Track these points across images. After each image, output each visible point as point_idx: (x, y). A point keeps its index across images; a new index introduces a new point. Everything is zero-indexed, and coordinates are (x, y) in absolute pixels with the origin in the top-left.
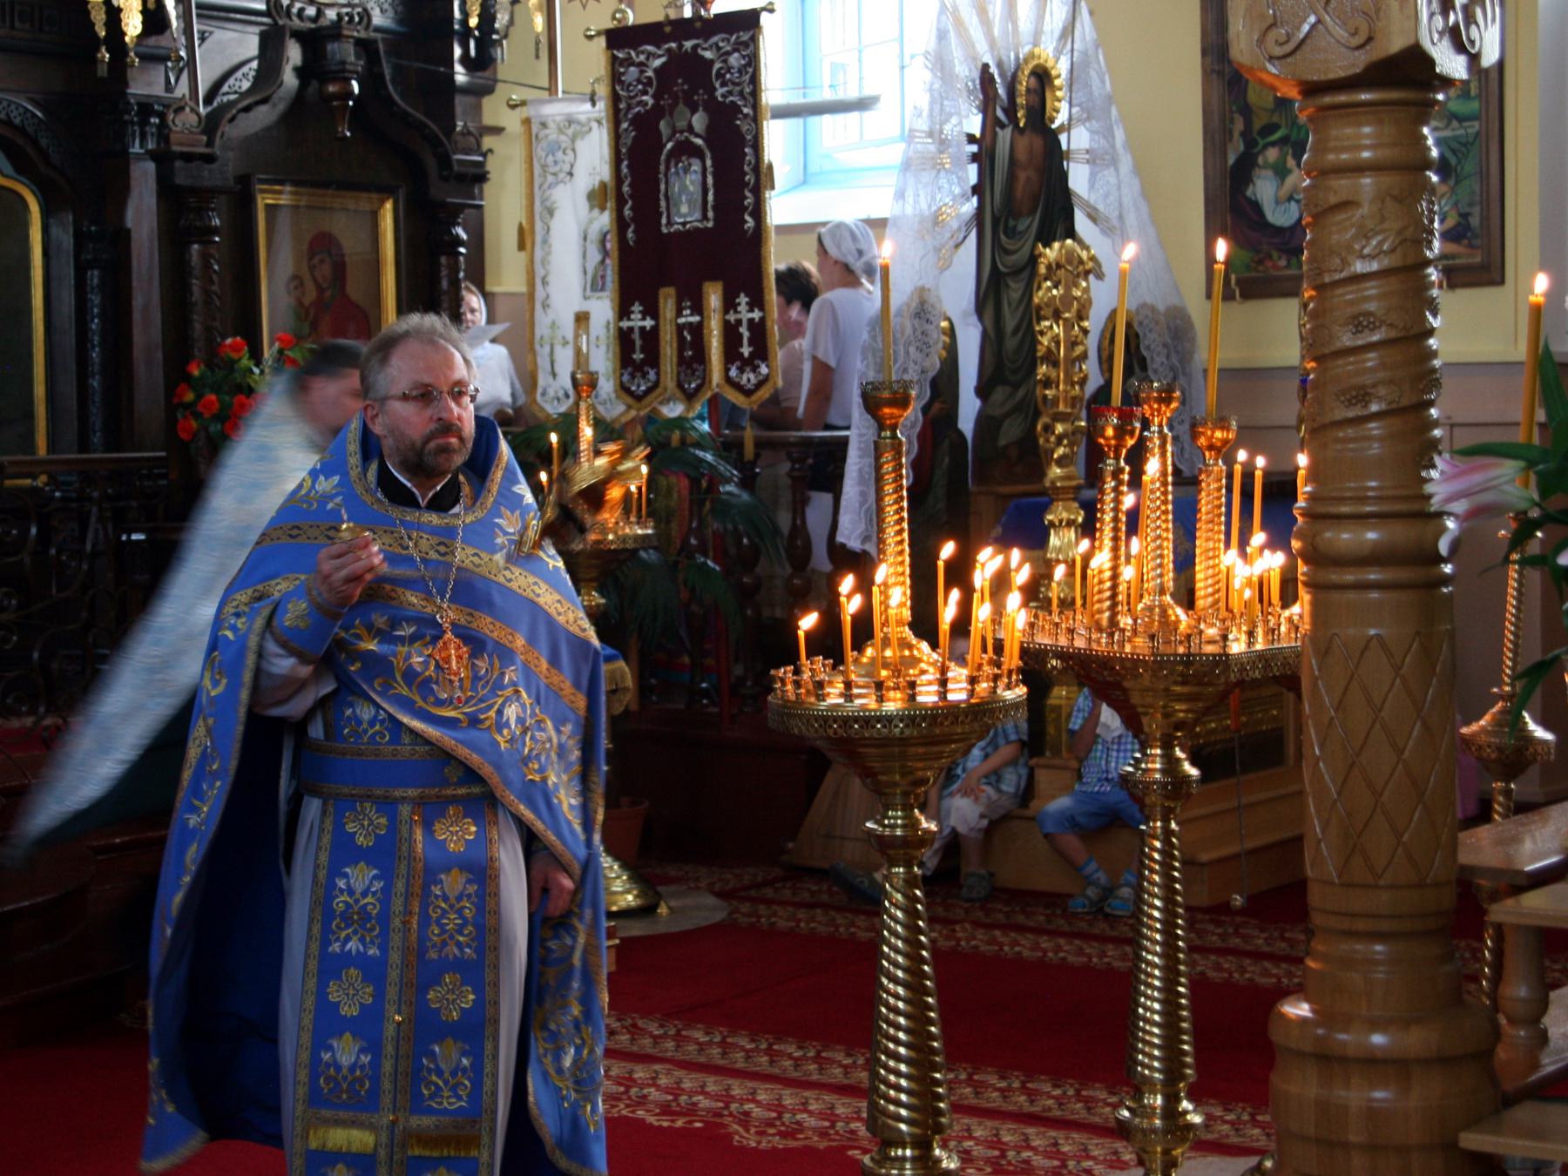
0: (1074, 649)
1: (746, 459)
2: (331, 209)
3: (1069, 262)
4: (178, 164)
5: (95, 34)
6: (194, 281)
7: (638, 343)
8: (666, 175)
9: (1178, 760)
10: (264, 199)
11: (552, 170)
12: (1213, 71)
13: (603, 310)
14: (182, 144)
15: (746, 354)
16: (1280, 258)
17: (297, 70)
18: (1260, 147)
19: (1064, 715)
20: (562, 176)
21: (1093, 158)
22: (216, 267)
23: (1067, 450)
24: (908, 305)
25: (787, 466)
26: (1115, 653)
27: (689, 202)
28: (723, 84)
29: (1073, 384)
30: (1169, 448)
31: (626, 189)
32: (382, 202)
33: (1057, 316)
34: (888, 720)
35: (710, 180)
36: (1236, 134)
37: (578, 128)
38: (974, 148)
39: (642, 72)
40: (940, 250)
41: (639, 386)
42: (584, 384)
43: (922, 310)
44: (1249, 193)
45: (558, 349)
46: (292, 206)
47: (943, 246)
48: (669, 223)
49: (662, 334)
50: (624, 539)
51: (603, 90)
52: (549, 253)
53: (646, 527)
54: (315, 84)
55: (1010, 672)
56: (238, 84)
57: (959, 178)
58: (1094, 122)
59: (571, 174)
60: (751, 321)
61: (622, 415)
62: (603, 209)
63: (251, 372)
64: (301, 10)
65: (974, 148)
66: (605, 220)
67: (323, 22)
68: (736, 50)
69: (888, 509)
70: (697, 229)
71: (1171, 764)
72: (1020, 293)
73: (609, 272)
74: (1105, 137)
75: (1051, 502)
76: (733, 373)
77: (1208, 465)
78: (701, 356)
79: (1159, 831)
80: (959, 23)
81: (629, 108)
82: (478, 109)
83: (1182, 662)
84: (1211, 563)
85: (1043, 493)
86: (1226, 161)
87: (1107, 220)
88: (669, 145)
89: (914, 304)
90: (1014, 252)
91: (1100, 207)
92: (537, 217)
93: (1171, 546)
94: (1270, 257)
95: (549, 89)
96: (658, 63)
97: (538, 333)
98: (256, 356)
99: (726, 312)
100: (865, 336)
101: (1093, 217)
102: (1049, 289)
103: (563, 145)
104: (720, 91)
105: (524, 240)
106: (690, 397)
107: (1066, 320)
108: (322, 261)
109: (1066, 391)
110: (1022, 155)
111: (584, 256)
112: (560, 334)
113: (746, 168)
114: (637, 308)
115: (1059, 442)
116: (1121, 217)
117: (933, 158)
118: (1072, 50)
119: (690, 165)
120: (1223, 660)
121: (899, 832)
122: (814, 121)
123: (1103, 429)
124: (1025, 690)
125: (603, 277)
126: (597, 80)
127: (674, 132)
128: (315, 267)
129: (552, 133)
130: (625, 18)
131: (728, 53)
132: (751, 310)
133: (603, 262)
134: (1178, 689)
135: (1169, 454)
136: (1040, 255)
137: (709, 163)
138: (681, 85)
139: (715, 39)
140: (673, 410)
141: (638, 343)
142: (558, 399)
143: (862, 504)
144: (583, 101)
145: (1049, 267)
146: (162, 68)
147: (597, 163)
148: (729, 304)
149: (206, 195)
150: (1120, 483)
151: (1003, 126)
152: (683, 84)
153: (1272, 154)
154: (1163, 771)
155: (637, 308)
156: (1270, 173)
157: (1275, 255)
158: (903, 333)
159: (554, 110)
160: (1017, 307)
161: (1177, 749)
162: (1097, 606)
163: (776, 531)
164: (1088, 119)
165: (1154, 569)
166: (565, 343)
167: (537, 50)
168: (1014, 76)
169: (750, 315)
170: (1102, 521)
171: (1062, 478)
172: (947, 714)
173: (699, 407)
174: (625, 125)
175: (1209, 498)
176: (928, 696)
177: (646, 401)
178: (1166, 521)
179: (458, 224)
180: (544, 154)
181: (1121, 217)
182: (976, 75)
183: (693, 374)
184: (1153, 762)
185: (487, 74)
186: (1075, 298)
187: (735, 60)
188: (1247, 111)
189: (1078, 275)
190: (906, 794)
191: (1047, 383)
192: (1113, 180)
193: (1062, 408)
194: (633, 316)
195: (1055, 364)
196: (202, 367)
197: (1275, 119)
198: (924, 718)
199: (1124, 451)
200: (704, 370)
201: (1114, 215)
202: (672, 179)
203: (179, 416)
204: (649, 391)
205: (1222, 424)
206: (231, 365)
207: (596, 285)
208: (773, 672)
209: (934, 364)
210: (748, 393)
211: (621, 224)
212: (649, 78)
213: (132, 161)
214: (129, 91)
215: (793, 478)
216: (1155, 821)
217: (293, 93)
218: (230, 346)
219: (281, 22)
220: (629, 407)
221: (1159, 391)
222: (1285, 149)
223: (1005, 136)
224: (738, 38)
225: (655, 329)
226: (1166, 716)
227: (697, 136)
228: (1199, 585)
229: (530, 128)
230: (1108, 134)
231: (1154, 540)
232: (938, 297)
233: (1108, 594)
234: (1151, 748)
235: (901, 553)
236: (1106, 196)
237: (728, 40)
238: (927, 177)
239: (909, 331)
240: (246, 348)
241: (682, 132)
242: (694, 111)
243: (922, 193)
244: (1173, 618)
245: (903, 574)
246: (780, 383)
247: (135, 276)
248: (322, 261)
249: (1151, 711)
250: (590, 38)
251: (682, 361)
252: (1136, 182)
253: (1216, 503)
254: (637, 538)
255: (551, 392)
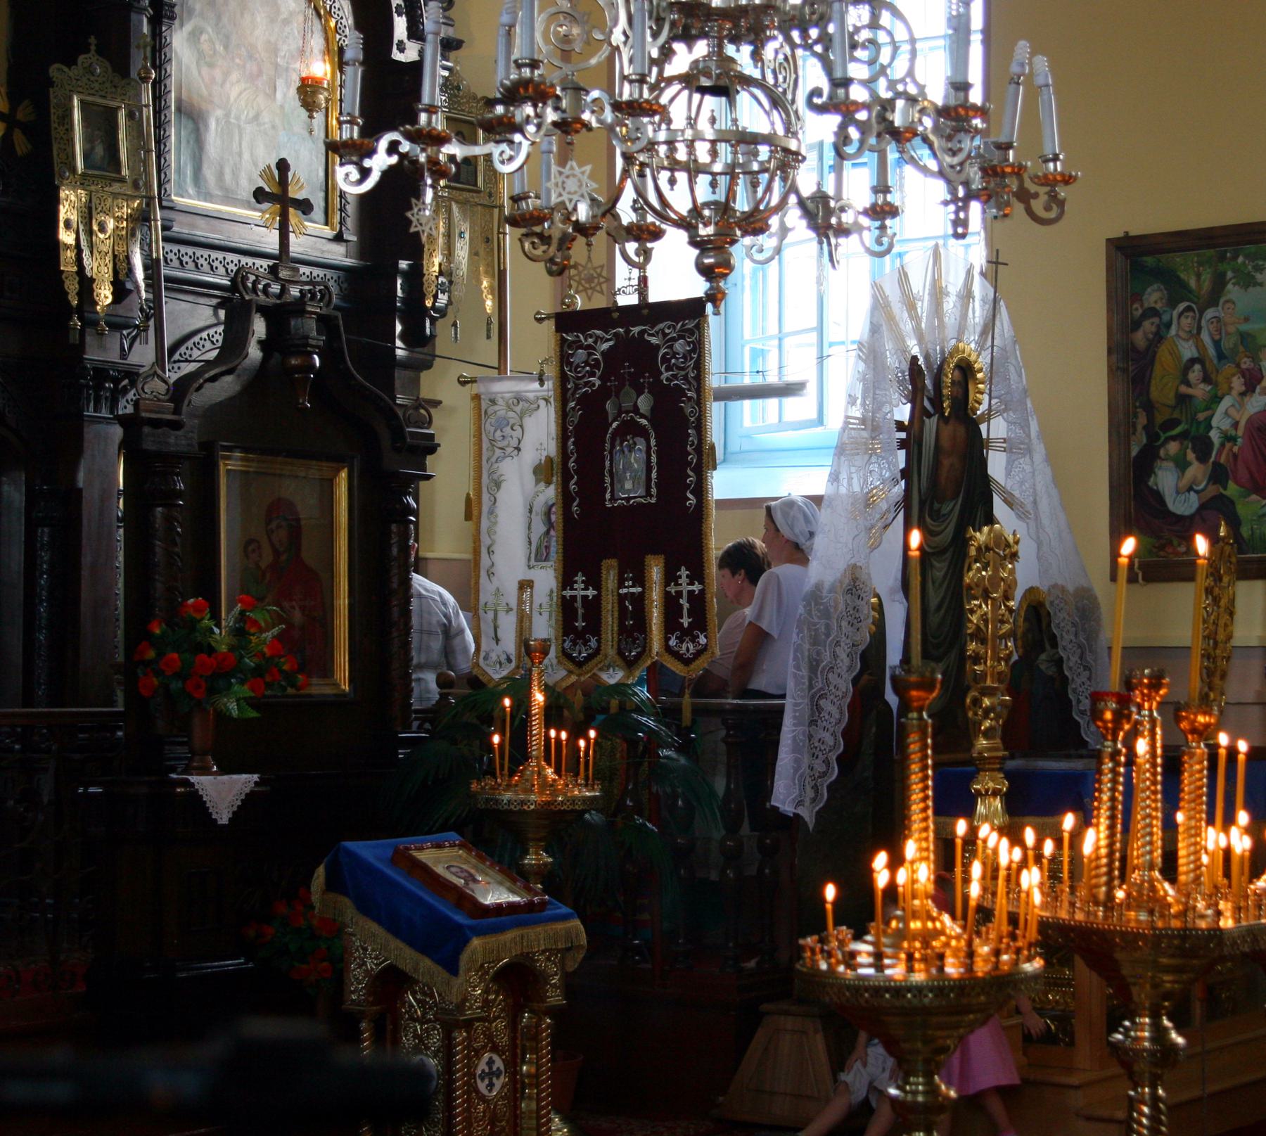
0: (1075, 921)
1: (684, 724)
2: (280, 475)
3: (998, 545)
4: (146, 430)
5: (68, 302)
6: (158, 543)
7: (686, 606)
8: (611, 453)
9: (1166, 1029)
10: (227, 465)
11: (500, 444)
12: (1118, 368)
13: (546, 579)
14: (151, 411)
15: (686, 625)
16: (1179, 545)
17: (260, 342)
18: (1162, 439)
19: (574, 936)
20: (509, 450)
21: (1009, 446)
22: (179, 530)
23: (993, 723)
24: (841, 582)
25: (723, 733)
26: (1115, 926)
27: (633, 479)
28: (667, 370)
29: (999, 660)
30: (1158, 731)
31: (571, 464)
32: (338, 471)
33: (986, 596)
34: (918, 990)
35: (654, 459)
36: (1139, 427)
37: (526, 405)
38: (903, 435)
39: (590, 354)
40: (870, 529)
41: (580, 653)
42: (529, 650)
43: (854, 585)
44: (1151, 483)
45: (501, 615)
46: (242, 472)
47: (873, 527)
48: (613, 499)
49: (604, 603)
50: (573, 800)
51: (551, 371)
52: (496, 523)
53: (593, 790)
54: (277, 357)
55: (1030, 945)
56: (188, 352)
57: (889, 463)
58: (1011, 413)
59: (518, 449)
60: (691, 593)
61: (562, 679)
62: (548, 483)
63: (212, 632)
64: (267, 286)
65: (903, 435)
66: (550, 493)
67: (287, 299)
68: (682, 337)
69: (914, 787)
70: (640, 504)
71: (1159, 1034)
72: (942, 573)
73: (553, 543)
74: (1022, 428)
75: (978, 771)
76: (673, 642)
77: (1190, 747)
78: (642, 624)
79: (1147, 1097)
80: (891, 318)
81: (577, 387)
82: (416, 382)
83: (1179, 936)
84: (1193, 840)
85: (971, 762)
86: (1129, 453)
87: (1022, 505)
88: (615, 425)
89: (847, 581)
90: (938, 534)
91: (1016, 493)
92: (484, 489)
93: (1159, 824)
94: (1171, 543)
95: (498, 369)
96: (605, 346)
97: (482, 600)
98: (216, 616)
99: (667, 584)
100: (801, 610)
101: (1009, 502)
102: (979, 570)
103: (512, 421)
104: (665, 375)
105: (471, 510)
106: (630, 664)
107: (993, 599)
108: (279, 527)
109: (993, 667)
110: (946, 443)
111: (529, 528)
112: (503, 601)
113: (689, 448)
114: (580, 578)
115: (986, 716)
116: (1035, 502)
117: (865, 444)
118: (993, 346)
119: (635, 444)
120: (1216, 934)
121: (920, 1099)
122: (734, 405)
123: (1102, 713)
124: (1042, 962)
125: (547, 548)
126: (546, 361)
127: (620, 413)
128: (273, 532)
129: (501, 409)
130: (574, 304)
131: (674, 340)
132: (692, 583)
133: (547, 532)
134: (1164, 960)
135: (1158, 737)
136: (971, 538)
137: (653, 442)
138: (627, 369)
139: (661, 326)
140: (613, 677)
141: (580, 611)
142: (500, 664)
143: (796, 770)
144: (532, 380)
145: (979, 549)
146: (118, 335)
147: (544, 439)
148: (670, 576)
149: (170, 459)
150: (1118, 764)
151: (929, 416)
152: (629, 367)
153: (1173, 447)
154: (1153, 1040)
155: (580, 578)
156: (1171, 465)
157: (1175, 542)
158: (836, 607)
159: (504, 388)
160: (941, 585)
161: (1164, 1018)
162: (1094, 881)
163: (713, 794)
164: (1005, 410)
165: (1144, 846)
166: (509, 610)
167: (489, 331)
168: (941, 368)
169: (691, 588)
170: (1099, 800)
171: (989, 750)
172: (967, 985)
173: (640, 672)
174: (572, 404)
175: (1194, 774)
176: (952, 969)
177: (586, 668)
178: (1155, 801)
179: (409, 494)
180: (492, 429)
181: (1035, 502)
182: (906, 366)
183: (634, 642)
184: (1143, 1030)
185: (425, 350)
186: (1002, 579)
187: (679, 346)
188: (1149, 407)
189: (1005, 558)
190: (927, 1061)
191: (977, 659)
192: (1028, 468)
193: (989, 683)
194: (576, 586)
195: (983, 641)
196: (164, 626)
197: (1176, 415)
198: (952, 989)
199: (1121, 734)
200: (645, 639)
201: (1028, 502)
202: (617, 457)
203: (139, 672)
204: (590, 658)
205: (1206, 710)
206: (192, 625)
207: (539, 555)
208: (801, 942)
209: (864, 637)
210: (687, 662)
211: (566, 497)
212: (596, 360)
213: (86, 424)
214: (86, 356)
215: (727, 743)
216: (1143, 1087)
217: (258, 363)
218: (193, 606)
219: (247, 298)
220: (570, 672)
221: (1150, 678)
222: (1186, 442)
223: (931, 424)
224: (683, 325)
225: (597, 598)
226: (1155, 986)
227: (642, 416)
228: (1181, 861)
229: (480, 404)
230: (1025, 426)
231: (1144, 819)
232: (869, 574)
233: (1104, 870)
234: (1140, 1016)
235: (926, 829)
236: (1022, 483)
237: (674, 328)
238: (859, 460)
239: (841, 607)
240: (208, 610)
241: (627, 412)
242: (640, 393)
243: (854, 476)
244: (1162, 893)
245: (927, 849)
246: (718, 653)
247: (84, 534)
248: (279, 527)
249: (1141, 981)
250: (540, 320)
251: (622, 629)
252: (1048, 470)
253: (1199, 783)
254: (585, 799)
255: (494, 656)
